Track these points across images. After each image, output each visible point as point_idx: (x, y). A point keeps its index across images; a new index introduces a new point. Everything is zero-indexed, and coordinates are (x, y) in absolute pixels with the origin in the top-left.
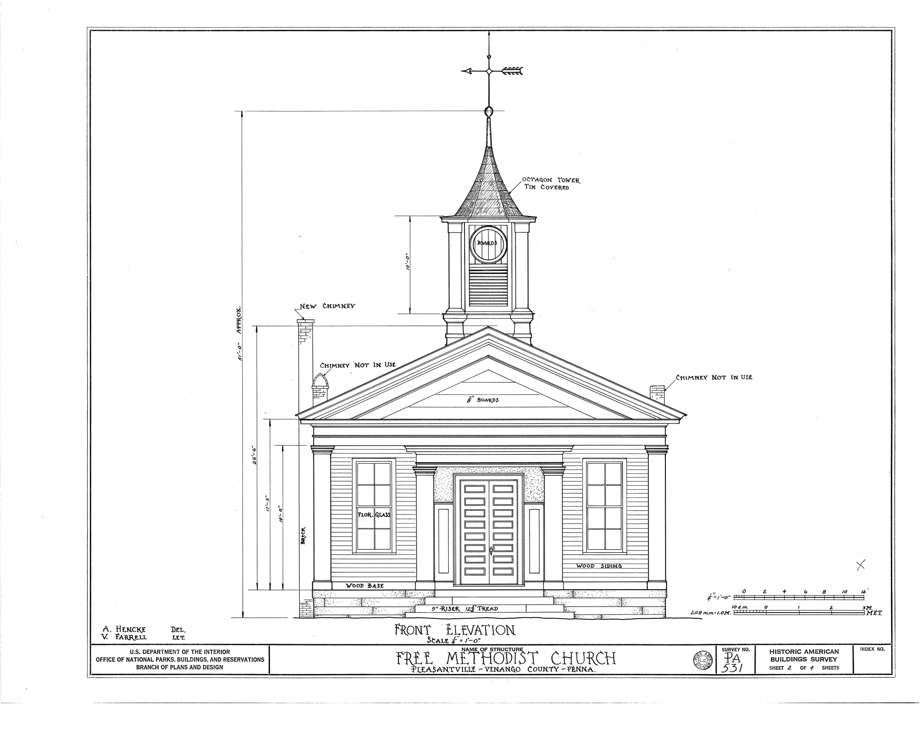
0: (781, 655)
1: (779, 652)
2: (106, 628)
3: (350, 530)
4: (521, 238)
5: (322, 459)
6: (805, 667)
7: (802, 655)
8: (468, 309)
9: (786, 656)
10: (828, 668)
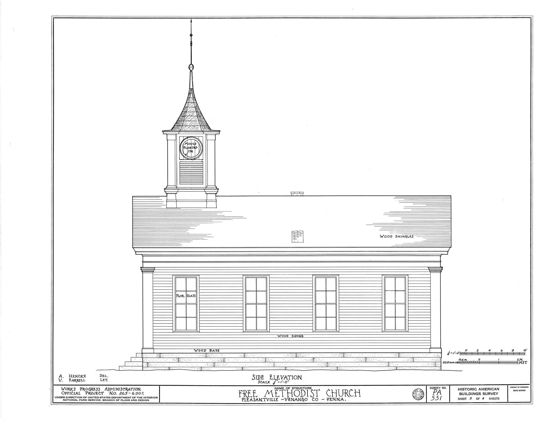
0: (465, 391)
1: (463, 389)
2: (61, 376)
3: (409, 316)
4: (211, 144)
5: (148, 276)
6: (479, 398)
7: (478, 391)
8: (179, 186)
9: (469, 393)
10: (493, 399)
